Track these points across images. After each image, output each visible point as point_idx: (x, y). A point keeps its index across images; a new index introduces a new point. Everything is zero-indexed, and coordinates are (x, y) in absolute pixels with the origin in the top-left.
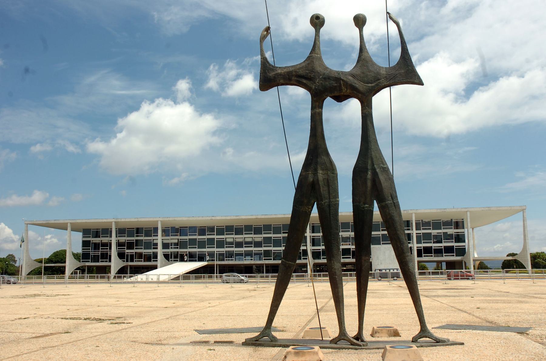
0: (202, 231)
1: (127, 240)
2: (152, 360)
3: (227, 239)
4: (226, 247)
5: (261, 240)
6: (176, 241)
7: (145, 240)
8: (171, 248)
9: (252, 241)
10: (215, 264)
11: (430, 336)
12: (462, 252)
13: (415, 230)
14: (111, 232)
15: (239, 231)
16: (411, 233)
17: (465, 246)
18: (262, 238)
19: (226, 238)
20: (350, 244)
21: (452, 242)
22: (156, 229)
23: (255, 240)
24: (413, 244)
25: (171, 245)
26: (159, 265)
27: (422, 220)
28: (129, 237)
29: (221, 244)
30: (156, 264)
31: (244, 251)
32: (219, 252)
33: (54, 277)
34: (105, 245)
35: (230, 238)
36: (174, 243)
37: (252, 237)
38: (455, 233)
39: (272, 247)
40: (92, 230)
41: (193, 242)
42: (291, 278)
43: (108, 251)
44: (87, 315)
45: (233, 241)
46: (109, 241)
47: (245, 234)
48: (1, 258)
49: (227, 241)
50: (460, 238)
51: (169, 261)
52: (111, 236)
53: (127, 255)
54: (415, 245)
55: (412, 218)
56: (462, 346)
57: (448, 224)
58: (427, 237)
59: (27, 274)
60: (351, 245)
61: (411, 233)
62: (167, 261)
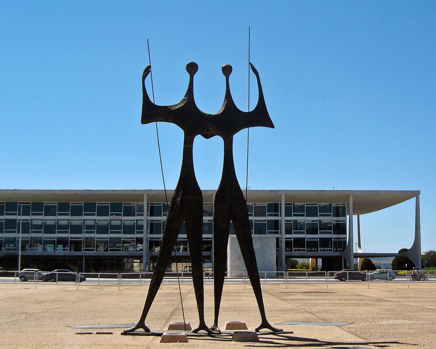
4: (32, 232)
5: (81, 224)
9: (41, 224)
10: (18, 256)
11: (269, 327)
15: (49, 211)
16: (279, 220)
18: (134, 221)
19: (32, 220)
21: (330, 233)
23: (98, 224)
24: (280, 234)
27: (294, 204)
28: (25, 215)
29: (26, 227)
31: (110, 238)
33: (367, 275)
35: (38, 219)
37: (122, 220)
39: (121, 233)
42: (164, 277)
45: (67, 224)
47: (59, 215)
50: (340, 228)
55: (281, 201)
57: (325, 210)
58: (129, 229)
61: (279, 220)
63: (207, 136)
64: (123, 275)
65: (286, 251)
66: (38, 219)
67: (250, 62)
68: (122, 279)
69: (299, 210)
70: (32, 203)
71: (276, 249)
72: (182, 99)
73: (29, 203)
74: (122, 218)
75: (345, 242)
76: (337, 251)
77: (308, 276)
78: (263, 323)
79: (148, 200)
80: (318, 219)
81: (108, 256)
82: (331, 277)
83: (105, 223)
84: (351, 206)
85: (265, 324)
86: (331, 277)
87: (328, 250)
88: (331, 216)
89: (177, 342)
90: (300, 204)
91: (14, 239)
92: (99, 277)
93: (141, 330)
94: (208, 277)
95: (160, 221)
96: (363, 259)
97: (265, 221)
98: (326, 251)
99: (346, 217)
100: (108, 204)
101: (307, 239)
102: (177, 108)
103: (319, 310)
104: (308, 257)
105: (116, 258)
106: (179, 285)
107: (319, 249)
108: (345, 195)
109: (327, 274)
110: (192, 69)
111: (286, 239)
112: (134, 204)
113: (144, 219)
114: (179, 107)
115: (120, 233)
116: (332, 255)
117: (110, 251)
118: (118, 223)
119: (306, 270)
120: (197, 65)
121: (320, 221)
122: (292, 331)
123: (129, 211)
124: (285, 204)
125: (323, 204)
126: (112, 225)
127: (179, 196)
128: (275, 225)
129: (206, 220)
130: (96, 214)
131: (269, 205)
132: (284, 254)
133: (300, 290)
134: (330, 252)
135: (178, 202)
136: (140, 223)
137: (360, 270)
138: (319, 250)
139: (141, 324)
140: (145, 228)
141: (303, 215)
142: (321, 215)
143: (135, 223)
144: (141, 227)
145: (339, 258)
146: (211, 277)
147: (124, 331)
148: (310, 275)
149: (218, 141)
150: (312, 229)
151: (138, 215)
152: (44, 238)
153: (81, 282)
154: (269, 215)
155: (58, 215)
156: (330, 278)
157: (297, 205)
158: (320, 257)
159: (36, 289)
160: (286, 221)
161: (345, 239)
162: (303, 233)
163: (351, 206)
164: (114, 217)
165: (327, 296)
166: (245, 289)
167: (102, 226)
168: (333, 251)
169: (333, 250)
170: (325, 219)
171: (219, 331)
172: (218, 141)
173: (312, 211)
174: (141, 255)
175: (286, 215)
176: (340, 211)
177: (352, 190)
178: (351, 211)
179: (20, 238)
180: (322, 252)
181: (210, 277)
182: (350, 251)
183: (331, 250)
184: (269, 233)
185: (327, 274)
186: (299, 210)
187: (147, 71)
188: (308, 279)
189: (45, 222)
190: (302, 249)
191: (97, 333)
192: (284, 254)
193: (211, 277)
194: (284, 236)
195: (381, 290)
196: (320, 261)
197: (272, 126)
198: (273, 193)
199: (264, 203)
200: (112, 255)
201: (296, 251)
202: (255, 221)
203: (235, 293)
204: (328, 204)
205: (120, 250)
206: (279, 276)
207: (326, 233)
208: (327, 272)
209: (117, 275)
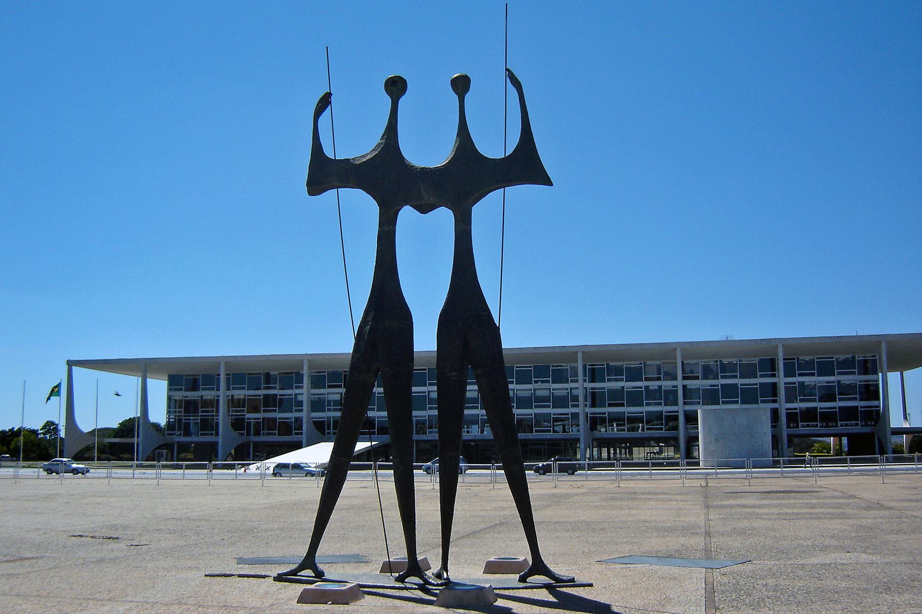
1: (248, 396)
7: (280, 395)
8: (329, 410)
12: (877, 417)
13: (304, 402)
14: (219, 379)
17: (677, 412)
22: (299, 377)
26: (304, 442)
27: (798, 358)
30: (216, 440)
34: (207, 403)
36: (333, 400)
38: (860, 381)
40: (184, 378)
43: (184, 416)
46: (184, 398)
48: (3, 432)
49: (431, 397)
50: (871, 392)
51: (324, 434)
52: (218, 390)
53: (249, 424)
54: (782, 406)
55: (777, 356)
56: (590, 588)
57: (847, 365)
58: (561, 402)
59: (146, 458)
60: (701, 403)
62: (321, 435)
63: (424, 209)
64: (561, 464)
65: (788, 427)
67: (507, 68)
69: (807, 367)
71: (770, 426)
72: (376, 144)
73: (425, 370)
74: (550, 386)
75: (879, 410)
76: (867, 425)
77: (652, 467)
78: (534, 565)
79: (584, 360)
81: (533, 440)
82: (852, 465)
83: (528, 394)
84: (884, 358)
85: (538, 567)
86: (852, 465)
87: (853, 424)
89: (326, 604)
90: (807, 358)
93: (309, 572)
94: (803, 466)
95: (604, 388)
96: (911, 436)
97: (756, 384)
98: (849, 426)
99: (878, 374)
100: (531, 367)
101: (820, 409)
102: (364, 160)
104: (829, 435)
105: (546, 442)
107: (839, 423)
108: (874, 342)
110: (394, 89)
111: (787, 409)
112: (566, 366)
113: (580, 386)
114: (368, 158)
115: (549, 406)
117: (536, 432)
118: (545, 393)
119: (826, 454)
120: (400, 77)
121: (839, 382)
122: (591, 583)
123: (560, 377)
124: (784, 359)
125: (842, 357)
127: (369, 322)
128: (773, 389)
129: (669, 386)
131: (761, 361)
132: (785, 432)
133: (767, 488)
134: (858, 428)
135: (365, 336)
136: (575, 392)
137: (907, 452)
138: (800, 426)
139: (309, 561)
140: (581, 399)
141: (813, 374)
142: (840, 374)
143: (568, 392)
144: (575, 398)
145: (871, 436)
146: (809, 466)
147: (278, 574)
148: (591, 467)
149: (444, 217)
150: (828, 395)
151: (572, 381)
154: (762, 376)
155: (429, 385)
156: (887, 465)
157: (804, 360)
158: (844, 435)
160: (785, 384)
161: (878, 407)
162: (814, 400)
163: (884, 358)
164: (539, 385)
165: (789, 498)
167: (523, 397)
168: (860, 425)
169: (861, 423)
170: (847, 379)
171: (448, 579)
172: (444, 217)
173: (825, 368)
174: (577, 437)
175: (786, 375)
176: (868, 366)
178: (885, 365)
179: (175, 410)
180: (843, 428)
181: (807, 466)
182: (885, 426)
183: (857, 425)
184: (763, 402)
186: (807, 367)
187: (325, 102)
188: (851, 468)
190: (813, 424)
191: (240, 576)
192: (785, 432)
193: (809, 466)
194: (784, 406)
195: (901, 485)
196: (845, 440)
197: (547, 181)
198: (764, 343)
199: (754, 359)
200: (540, 437)
201: (805, 427)
202: (741, 385)
203: (649, 494)
204: (849, 356)
205: (550, 431)
206: (775, 464)
207: (849, 399)
208: (881, 457)
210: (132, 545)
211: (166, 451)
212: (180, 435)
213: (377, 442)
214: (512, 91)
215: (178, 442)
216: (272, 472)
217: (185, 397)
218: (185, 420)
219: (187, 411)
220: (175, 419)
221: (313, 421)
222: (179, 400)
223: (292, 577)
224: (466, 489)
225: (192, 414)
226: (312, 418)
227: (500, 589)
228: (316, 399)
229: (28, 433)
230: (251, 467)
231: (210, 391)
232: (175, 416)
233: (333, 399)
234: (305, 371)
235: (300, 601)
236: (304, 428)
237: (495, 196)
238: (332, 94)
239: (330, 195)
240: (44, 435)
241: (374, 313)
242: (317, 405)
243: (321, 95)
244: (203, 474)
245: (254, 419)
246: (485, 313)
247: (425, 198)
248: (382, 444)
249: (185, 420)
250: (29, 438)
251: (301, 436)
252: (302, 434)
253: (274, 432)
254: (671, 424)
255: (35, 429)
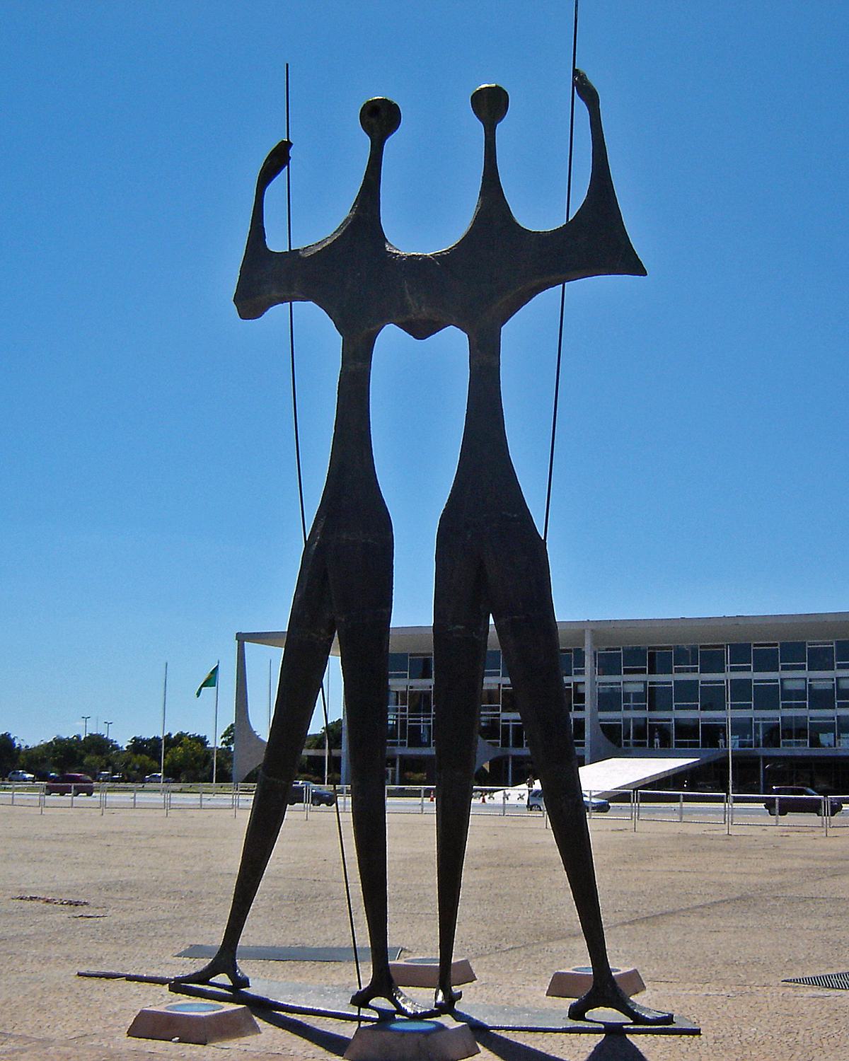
0: (711, 659)
2: (92, 1059)
3: (841, 682)
5: (831, 688)
6: (639, 688)
8: (627, 708)
10: (325, 757)
18: (833, 680)
20: (810, 681)
25: (627, 699)
26: (587, 757)
32: (763, 719)
35: (795, 678)
37: (805, 679)
41: (686, 692)
44: (601, 889)
51: (620, 746)
53: (506, 728)
63: (421, 329)
66: (795, 678)
67: (576, 68)
68: (641, 805)
70: (782, 644)
73: (776, 645)
80: (675, 677)
88: (406, 677)
89: (171, 1041)
91: (642, 723)
92: (681, 800)
103: (782, 874)
106: (336, 814)
109: (634, 796)
110: (373, 121)
116: (805, 754)
126: (785, 691)
130: (807, 666)
139: (226, 958)
150: (653, 698)
152: (811, 719)
153: (833, 815)
159: (307, 820)
166: (42, 816)
177: (726, 616)
185: (634, 796)
187: (279, 159)
189: (811, 685)
208: (634, 792)
209: (820, 800)
210: (82, 916)
211: (392, 768)
212: (403, 744)
213: (698, 759)
214: (582, 108)
215: (401, 756)
216: (526, 804)
217: (411, 687)
218: (410, 722)
219: (415, 709)
220: (397, 721)
221: (601, 725)
222: (402, 691)
223: (195, 986)
224: (782, 836)
225: (422, 714)
226: (600, 720)
227: (507, 1029)
228: (607, 691)
229: (189, 741)
230: (495, 795)
231: (402, 680)
232: (397, 716)
233: (634, 691)
234: (588, 649)
235: (131, 1033)
236: (587, 735)
237: (546, 300)
238: (291, 144)
239: (278, 312)
240: (226, 745)
241: (326, 519)
242: (608, 700)
243: (274, 145)
244: (415, 805)
245: (514, 721)
246: (515, 515)
247: (414, 309)
248: (705, 762)
249: (410, 722)
250: (191, 749)
251: (581, 748)
252: (584, 746)
253: (643, 741)
254: (786, 734)
255: (201, 735)
